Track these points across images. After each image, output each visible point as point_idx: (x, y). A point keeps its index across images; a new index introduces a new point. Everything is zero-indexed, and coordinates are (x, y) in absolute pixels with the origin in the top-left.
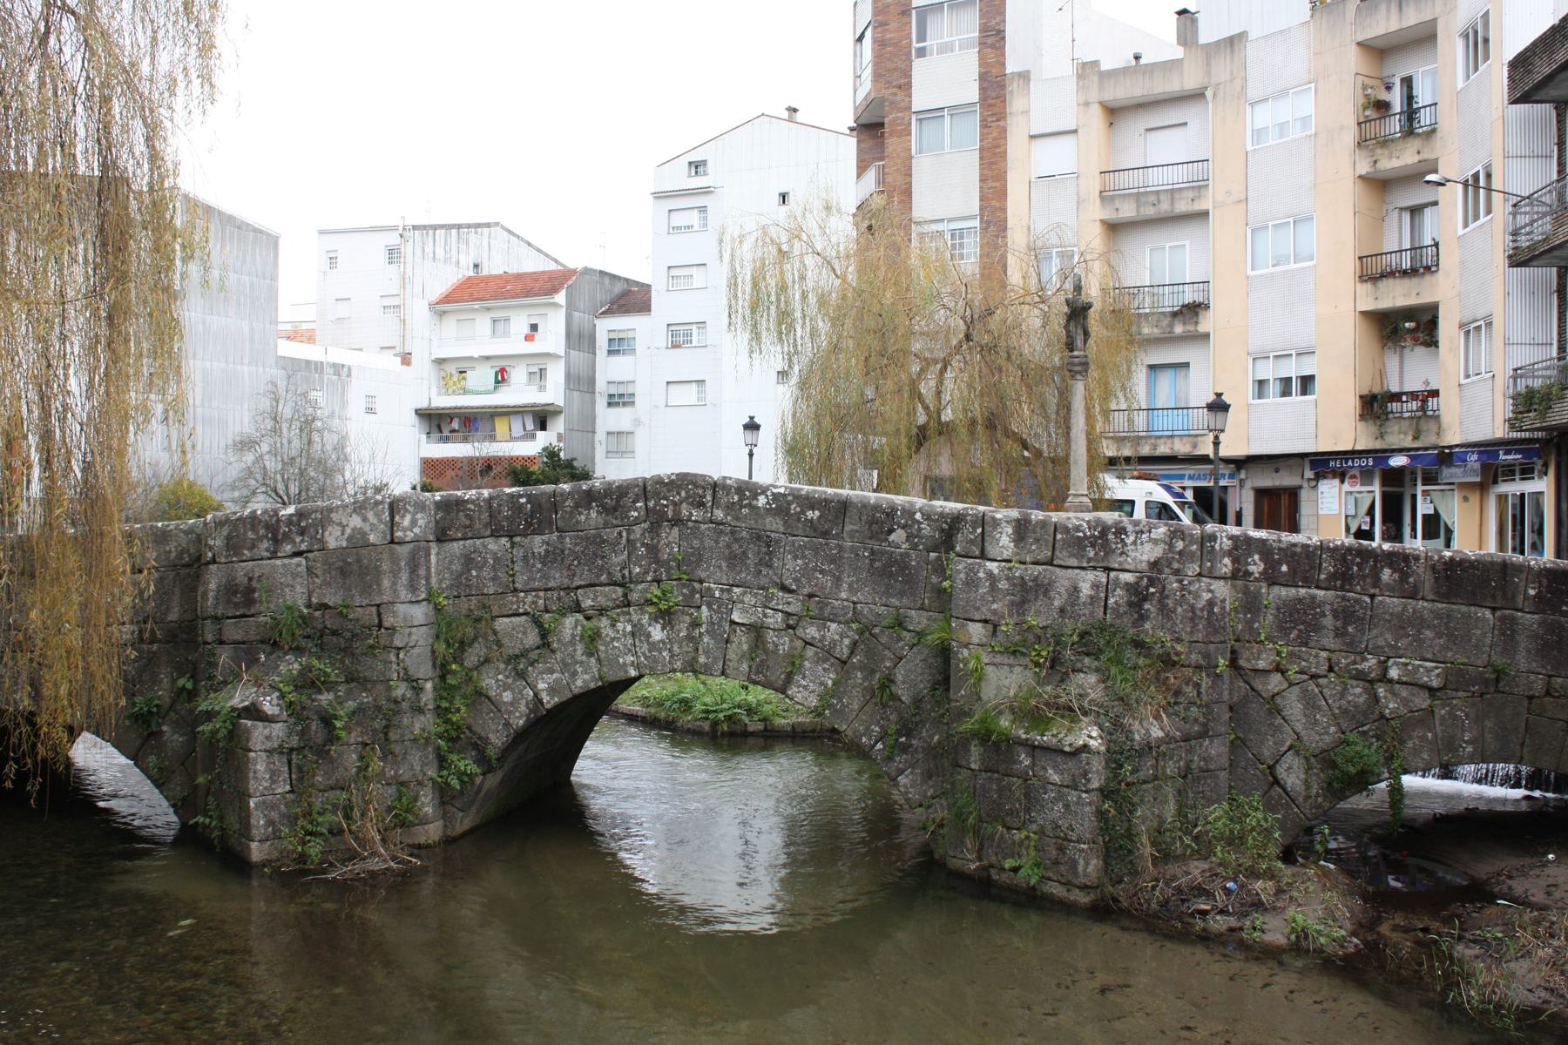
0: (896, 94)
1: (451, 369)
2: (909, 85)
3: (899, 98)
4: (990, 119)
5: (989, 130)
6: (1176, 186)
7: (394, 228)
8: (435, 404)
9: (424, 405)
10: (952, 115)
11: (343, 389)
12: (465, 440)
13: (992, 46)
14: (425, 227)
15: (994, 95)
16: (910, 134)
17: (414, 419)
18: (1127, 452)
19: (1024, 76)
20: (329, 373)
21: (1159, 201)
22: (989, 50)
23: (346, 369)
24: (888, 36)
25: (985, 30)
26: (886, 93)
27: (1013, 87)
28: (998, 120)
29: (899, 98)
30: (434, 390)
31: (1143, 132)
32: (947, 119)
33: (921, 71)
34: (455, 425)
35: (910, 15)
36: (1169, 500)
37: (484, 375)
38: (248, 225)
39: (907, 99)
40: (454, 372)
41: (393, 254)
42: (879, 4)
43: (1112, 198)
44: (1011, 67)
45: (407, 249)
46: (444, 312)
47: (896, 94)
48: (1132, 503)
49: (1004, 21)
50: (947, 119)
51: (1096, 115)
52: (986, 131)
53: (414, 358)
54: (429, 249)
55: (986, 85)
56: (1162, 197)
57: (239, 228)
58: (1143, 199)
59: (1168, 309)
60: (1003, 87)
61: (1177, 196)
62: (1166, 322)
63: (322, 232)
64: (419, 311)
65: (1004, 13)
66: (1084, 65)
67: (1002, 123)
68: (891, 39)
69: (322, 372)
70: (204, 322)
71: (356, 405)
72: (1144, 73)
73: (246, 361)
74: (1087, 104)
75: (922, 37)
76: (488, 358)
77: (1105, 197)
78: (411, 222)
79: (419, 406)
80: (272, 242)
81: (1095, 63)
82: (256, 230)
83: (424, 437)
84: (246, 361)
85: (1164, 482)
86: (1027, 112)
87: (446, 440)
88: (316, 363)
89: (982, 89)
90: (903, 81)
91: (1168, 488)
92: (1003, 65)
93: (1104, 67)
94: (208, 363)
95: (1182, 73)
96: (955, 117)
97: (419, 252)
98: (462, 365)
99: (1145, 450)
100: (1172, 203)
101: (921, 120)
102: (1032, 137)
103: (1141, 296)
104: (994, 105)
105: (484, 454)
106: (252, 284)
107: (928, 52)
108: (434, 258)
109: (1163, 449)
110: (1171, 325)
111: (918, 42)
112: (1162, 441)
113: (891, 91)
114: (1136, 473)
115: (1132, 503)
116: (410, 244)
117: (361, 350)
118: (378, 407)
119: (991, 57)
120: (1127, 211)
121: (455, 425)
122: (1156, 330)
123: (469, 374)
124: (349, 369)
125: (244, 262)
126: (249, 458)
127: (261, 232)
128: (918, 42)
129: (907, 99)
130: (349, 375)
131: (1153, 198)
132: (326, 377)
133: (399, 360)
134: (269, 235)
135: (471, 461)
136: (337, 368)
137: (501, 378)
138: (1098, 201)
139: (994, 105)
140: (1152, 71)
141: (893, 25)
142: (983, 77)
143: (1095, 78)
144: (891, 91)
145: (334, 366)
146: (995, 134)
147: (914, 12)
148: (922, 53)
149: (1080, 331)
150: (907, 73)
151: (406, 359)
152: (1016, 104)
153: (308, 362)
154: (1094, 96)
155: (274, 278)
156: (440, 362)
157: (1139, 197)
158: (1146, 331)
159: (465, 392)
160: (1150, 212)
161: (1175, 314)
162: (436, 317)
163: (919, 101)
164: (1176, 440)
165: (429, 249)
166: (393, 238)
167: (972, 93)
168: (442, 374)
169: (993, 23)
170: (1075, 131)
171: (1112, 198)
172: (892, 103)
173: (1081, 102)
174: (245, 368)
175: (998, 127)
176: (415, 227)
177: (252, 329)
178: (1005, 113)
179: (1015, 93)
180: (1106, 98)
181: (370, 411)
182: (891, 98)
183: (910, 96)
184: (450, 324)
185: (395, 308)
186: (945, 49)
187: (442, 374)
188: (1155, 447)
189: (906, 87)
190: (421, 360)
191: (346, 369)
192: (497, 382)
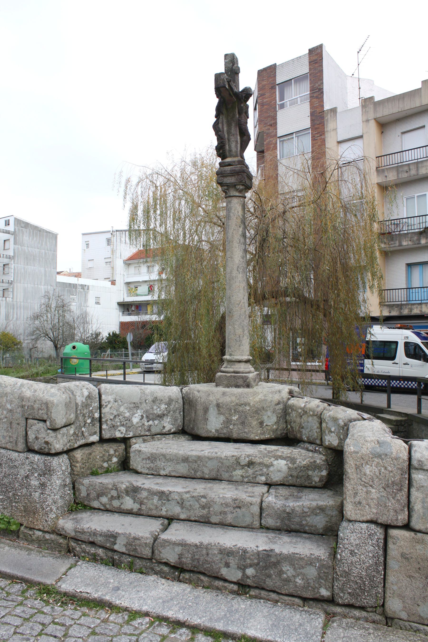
0: (269, 129)
1: (132, 286)
2: (275, 124)
3: (271, 131)
4: (316, 136)
5: (316, 141)
6: (419, 160)
7: (109, 232)
8: (126, 300)
9: (121, 300)
10: (298, 137)
11: (85, 294)
12: (138, 314)
13: (317, 97)
14: (121, 231)
15: (318, 123)
16: (276, 148)
17: (116, 306)
18: (394, 313)
19: (334, 111)
20: (79, 289)
21: (410, 170)
22: (315, 100)
23: (87, 287)
24: (265, 100)
25: (312, 90)
26: (264, 129)
27: (328, 117)
28: (321, 135)
29: (271, 131)
30: (126, 295)
31: (400, 134)
32: (295, 139)
33: (281, 115)
34: (133, 308)
35: (275, 88)
36: (417, 340)
37: (144, 289)
38: (44, 230)
39: (275, 131)
40: (133, 287)
41: (109, 241)
42: (261, 85)
43: (383, 171)
44: (327, 107)
45: (114, 239)
46: (130, 264)
47: (269, 129)
48: (397, 343)
49: (322, 83)
50: (295, 139)
51: (373, 127)
52: (315, 142)
53: (117, 283)
54: (123, 239)
55: (314, 118)
56: (411, 167)
57: (40, 231)
58: (400, 169)
59: (417, 230)
60: (323, 118)
61: (420, 165)
62: (415, 238)
63: (83, 234)
64: (119, 264)
65: (322, 79)
66: (365, 100)
67: (323, 137)
68: (266, 102)
69: (76, 288)
70: (24, 268)
71: (91, 301)
72: (399, 100)
73: (43, 284)
74: (367, 121)
75: (282, 98)
76: (146, 282)
77: (379, 170)
78: (115, 229)
79: (119, 301)
80: (54, 236)
81: (372, 98)
82: (47, 232)
83: (121, 313)
84: (43, 284)
85: (416, 331)
86: (335, 130)
87: (130, 314)
88: (74, 284)
89: (312, 121)
90: (272, 122)
91: (418, 334)
92: (323, 106)
93: (376, 99)
94: (26, 285)
95: (421, 96)
96: (300, 138)
97: (119, 240)
98: (136, 285)
99: (405, 312)
100: (417, 170)
101: (283, 141)
102: (339, 142)
103: (401, 225)
104: (319, 128)
105: (142, 320)
106: (45, 253)
107: (285, 106)
108: (125, 243)
109: (416, 311)
110: (419, 240)
111: (280, 101)
112: (415, 306)
113: (267, 128)
114: (399, 325)
115: (397, 343)
116: (115, 237)
117: (97, 279)
118: (101, 301)
119: (316, 104)
120: (392, 177)
121: (133, 308)
122: (410, 243)
123: (139, 288)
124: (88, 286)
125: (42, 245)
126: (37, 322)
127: (49, 233)
128: (280, 101)
129: (275, 131)
130: (88, 289)
131: (406, 168)
132: (78, 290)
133: (110, 283)
134: (53, 234)
135: (138, 322)
136: (83, 286)
137: (151, 289)
138: (375, 173)
139: (319, 128)
140: (403, 98)
141: (267, 95)
142: (312, 114)
143: (372, 106)
144: (267, 128)
145: (82, 285)
146: (319, 143)
147: (277, 87)
148: (282, 106)
149: (235, 131)
150: (275, 118)
151: (113, 283)
152: (330, 126)
153: (70, 284)
154: (371, 115)
155: (55, 251)
156: (128, 284)
157: (398, 168)
158: (404, 243)
159: (137, 295)
160: (404, 176)
161: (421, 233)
162: (127, 266)
163: (280, 133)
164: (424, 306)
165: (123, 239)
166: (109, 236)
167: (307, 123)
168: (129, 288)
169: (317, 85)
170: (361, 137)
171: (383, 171)
172: (267, 134)
173: (364, 120)
174: (42, 287)
175: (321, 139)
176: (117, 231)
177: (45, 271)
178: (324, 131)
179: (329, 120)
180: (378, 116)
181: (98, 303)
182: (267, 131)
183: (276, 129)
184: (132, 269)
185: (109, 263)
186: (293, 103)
187: (129, 288)
188: (411, 310)
189: (274, 125)
190: (120, 282)
191: (87, 287)
192: (149, 291)
